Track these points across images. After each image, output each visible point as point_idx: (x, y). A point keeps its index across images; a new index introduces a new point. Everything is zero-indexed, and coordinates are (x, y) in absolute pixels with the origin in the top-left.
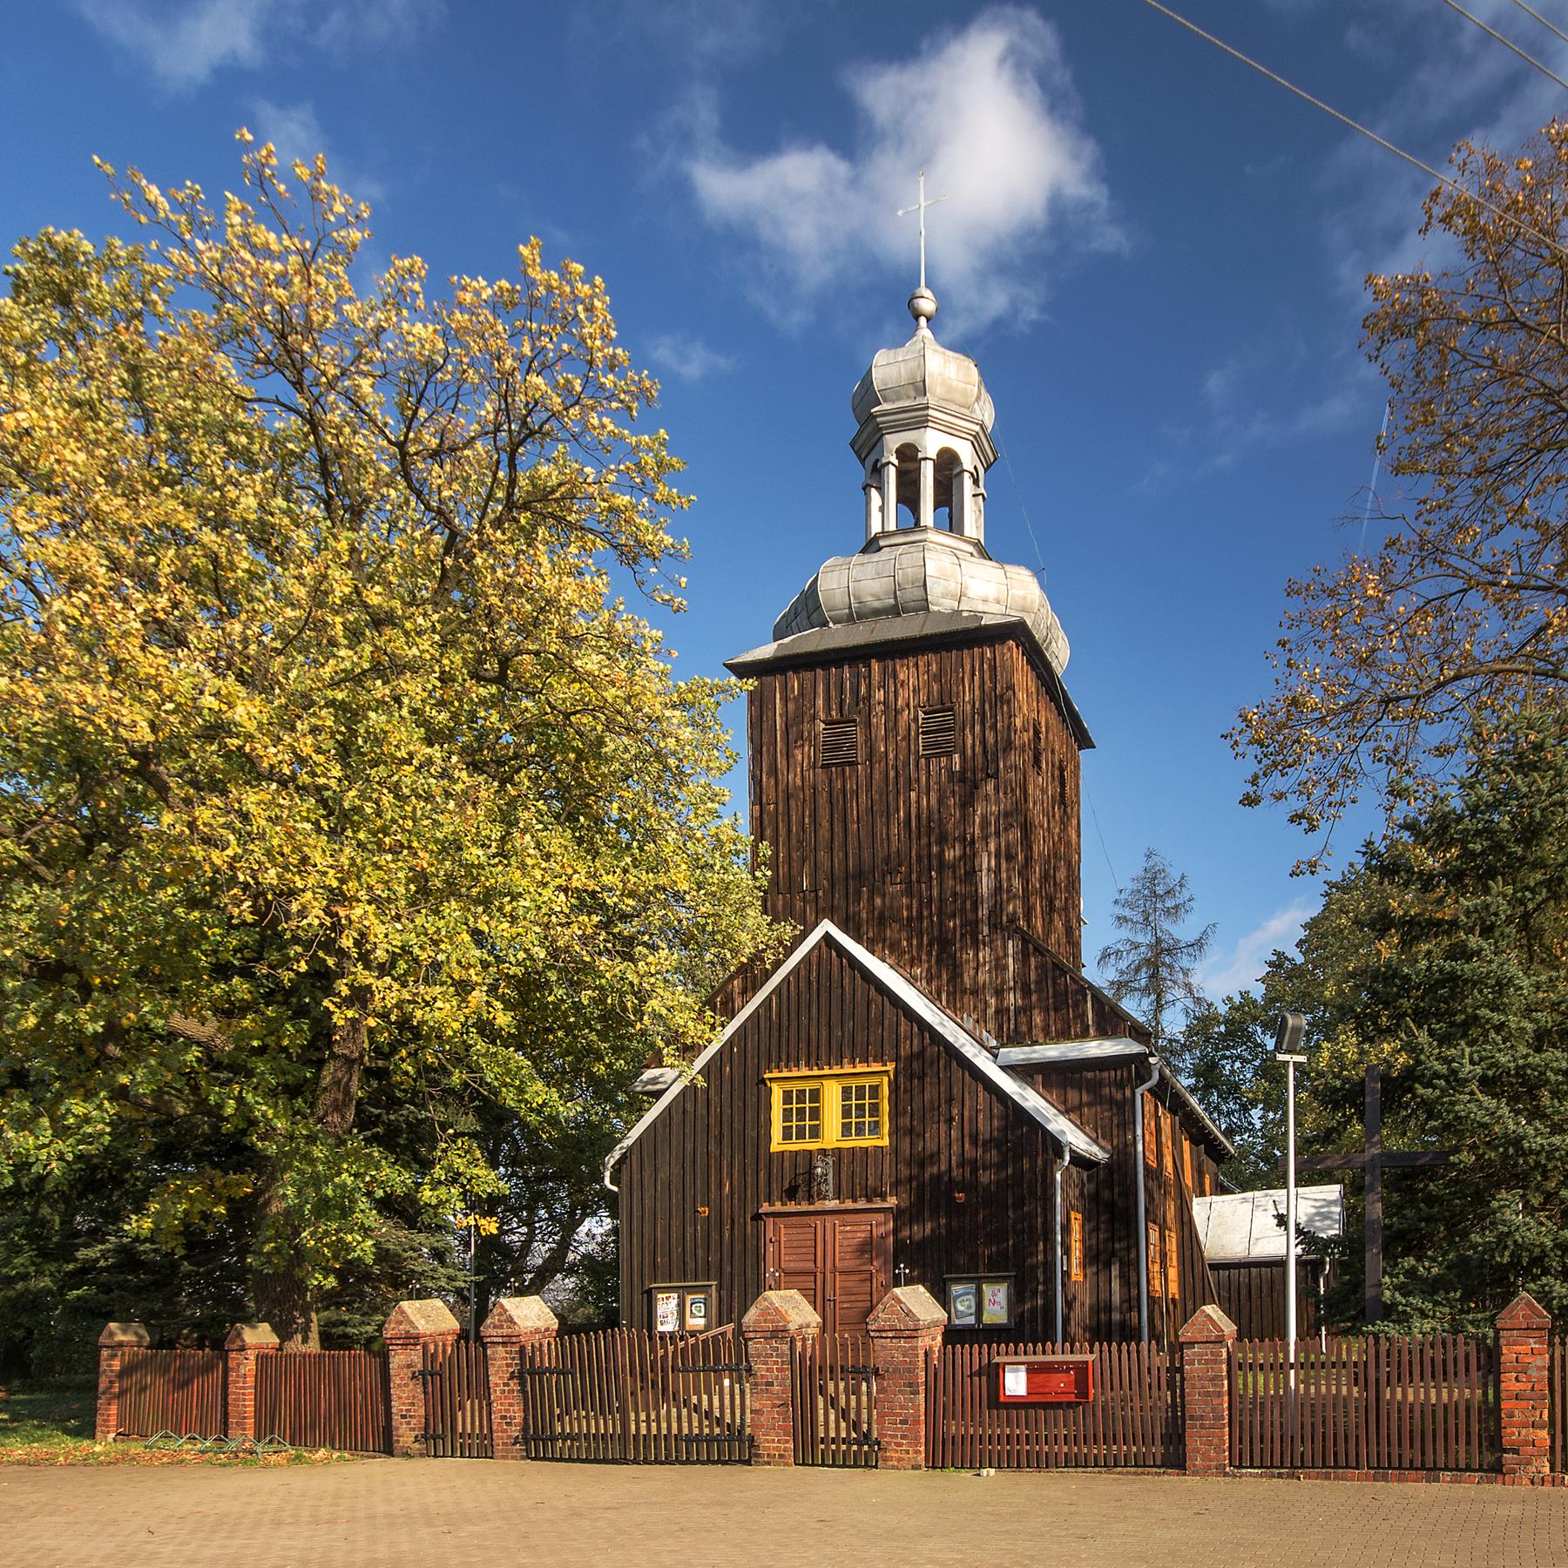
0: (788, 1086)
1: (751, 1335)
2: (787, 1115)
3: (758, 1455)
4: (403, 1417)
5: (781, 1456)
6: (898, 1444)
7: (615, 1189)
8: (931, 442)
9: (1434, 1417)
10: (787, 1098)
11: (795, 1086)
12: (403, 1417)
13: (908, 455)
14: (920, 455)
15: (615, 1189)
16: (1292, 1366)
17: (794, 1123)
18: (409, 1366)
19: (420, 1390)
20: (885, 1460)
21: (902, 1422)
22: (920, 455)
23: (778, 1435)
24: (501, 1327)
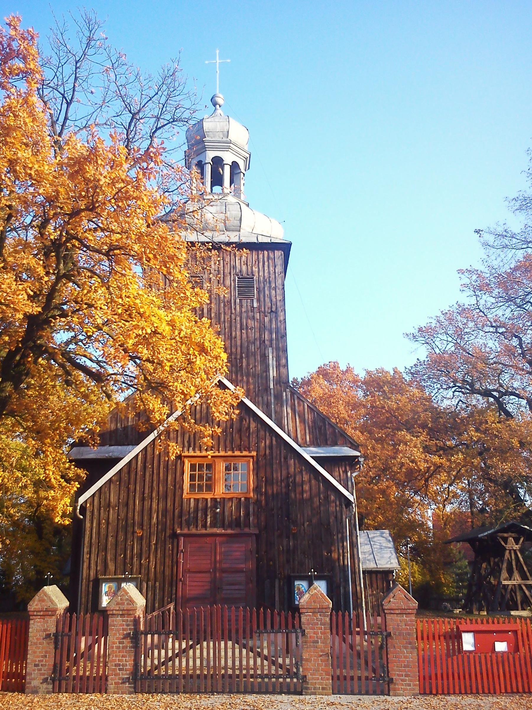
0: (194, 461)
1: (304, 611)
2: (192, 478)
3: (307, 688)
4: (36, 665)
5: (323, 689)
6: (402, 680)
7: (82, 517)
8: (228, 158)
9: (515, 665)
10: (193, 467)
11: (194, 461)
12: (36, 665)
13: (218, 162)
14: (224, 162)
15: (82, 517)
16: (142, 633)
17: (197, 482)
18: (45, 630)
19: (52, 646)
20: (395, 690)
21: (405, 666)
22: (224, 162)
23: (321, 675)
24: (123, 604)
